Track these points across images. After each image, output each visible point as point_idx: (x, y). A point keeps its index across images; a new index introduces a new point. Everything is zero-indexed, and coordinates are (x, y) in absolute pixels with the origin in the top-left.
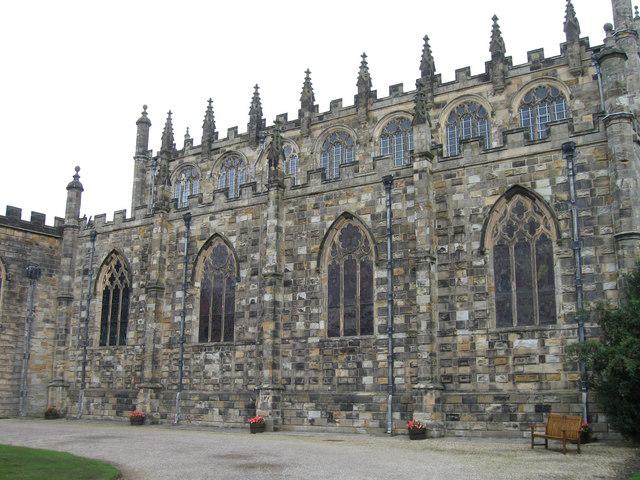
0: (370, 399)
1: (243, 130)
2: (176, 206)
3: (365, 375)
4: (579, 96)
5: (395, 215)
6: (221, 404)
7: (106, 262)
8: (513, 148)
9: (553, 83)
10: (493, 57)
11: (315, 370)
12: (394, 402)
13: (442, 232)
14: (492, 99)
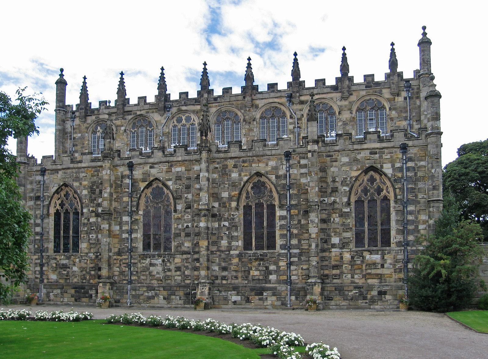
0: (275, 288)
1: (151, 99)
2: (119, 155)
3: (271, 274)
4: (395, 109)
5: (292, 177)
6: (165, 293)
7: (57, 192)
8: (370, 142)
9: (379, 98)
10: (342, 75)
11: (236, 271)
12: (291, 290)
13: (323, 190)
14: (339, 103)
